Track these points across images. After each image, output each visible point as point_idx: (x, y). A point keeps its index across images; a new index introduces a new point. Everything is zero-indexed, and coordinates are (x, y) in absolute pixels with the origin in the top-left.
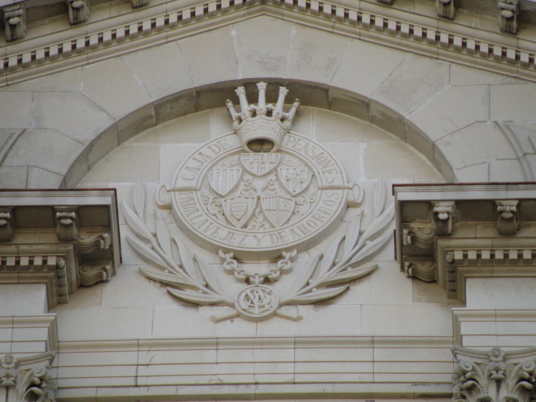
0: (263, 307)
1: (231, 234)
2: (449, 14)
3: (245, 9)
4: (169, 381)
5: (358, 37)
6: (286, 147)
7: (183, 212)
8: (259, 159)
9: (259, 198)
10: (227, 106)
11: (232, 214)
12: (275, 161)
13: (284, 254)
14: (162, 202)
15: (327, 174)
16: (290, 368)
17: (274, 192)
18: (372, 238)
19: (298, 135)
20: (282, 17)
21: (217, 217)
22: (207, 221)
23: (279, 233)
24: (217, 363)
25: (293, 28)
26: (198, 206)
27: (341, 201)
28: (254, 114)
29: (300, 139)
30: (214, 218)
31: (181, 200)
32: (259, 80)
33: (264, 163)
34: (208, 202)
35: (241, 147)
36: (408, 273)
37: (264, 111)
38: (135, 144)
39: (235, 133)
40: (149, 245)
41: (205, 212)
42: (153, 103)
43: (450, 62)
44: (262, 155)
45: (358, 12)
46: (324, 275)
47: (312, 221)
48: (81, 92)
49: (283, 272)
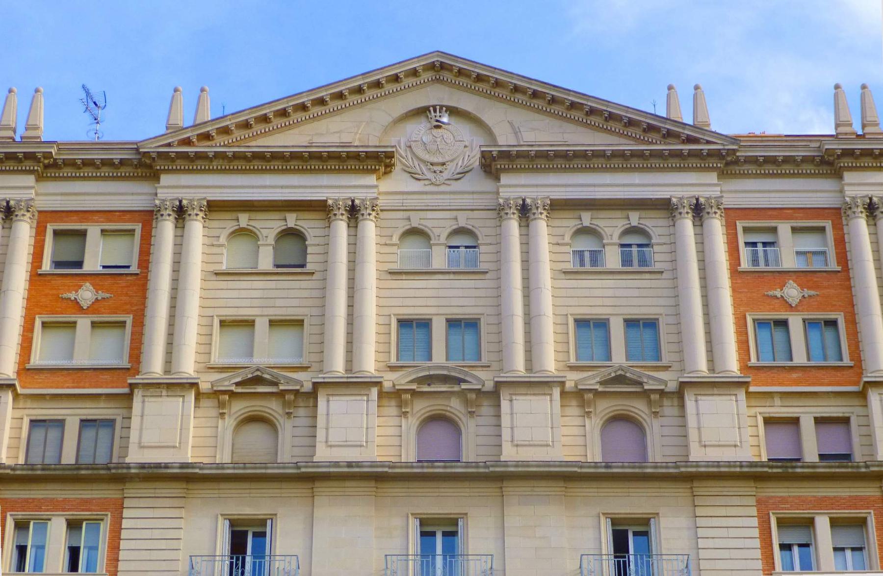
4: (413, 204)
16: (449, 201)
32: (437, 105)
46: (458, 170)
49: (446, 169)
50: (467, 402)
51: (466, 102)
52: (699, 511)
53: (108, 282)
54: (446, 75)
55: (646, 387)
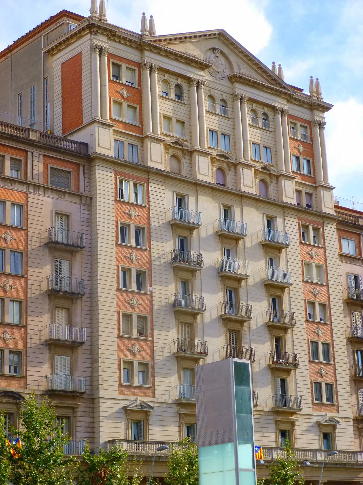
50: (228, 165)
51: (226, 51)
52: (286, 218)
53: (130, 89)
54: (221, 38)
55: (271, 173)
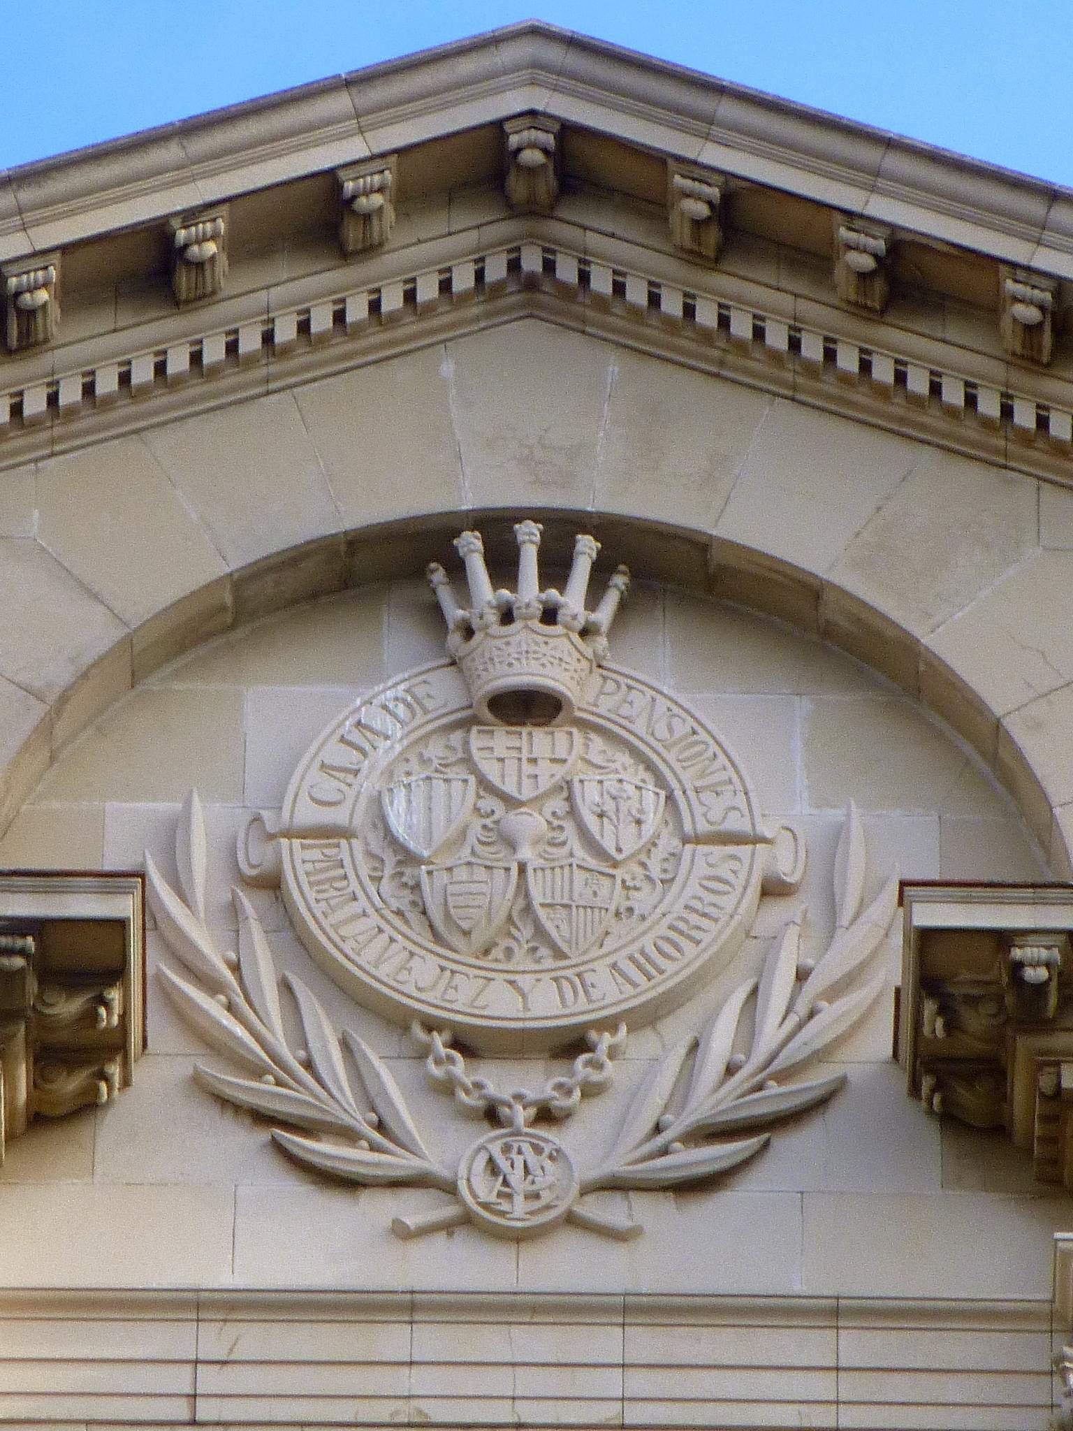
0: (537, 1196)
1: (448, 973)
2: (1040, 351)
3: (479, 303)
5: (789, 393)
6: (594, 709)
7: (313, 904)
8: (519, 749)
9: (522, 869)
10: (431, 581)
11: (447, 915)
12: (564, 756)
13: (593, 1035)
14: (254, 867)
15: (707, 797)
17: (564, 851)
18: (835, 991)
19: (627, 676)
20: (581, 327)
21: (407, 922)
22: (380, 931)
23: (579, 975)
24: (411, 1363)
25: (613, 357)
26: (354, 886)
27: (748, 881)
28: (507, 616)
29: (630, 688)
30: (397, 922)
31: (309, 867)
32: (520, 515)
33: (533, 761)
34: (383, 871)
35: (470, 707)
36: (931, 1103)
37: (537, 609)
38: (178, 686)
39: (453, 663)
40: (222, 998)
41: (373, 905)
42: (231, 575)
43: (1039, 478)
44: (530, 734)
45: (790, 327)
47: (668, 940)
48: (35, 540)
49: (591, 1091)
